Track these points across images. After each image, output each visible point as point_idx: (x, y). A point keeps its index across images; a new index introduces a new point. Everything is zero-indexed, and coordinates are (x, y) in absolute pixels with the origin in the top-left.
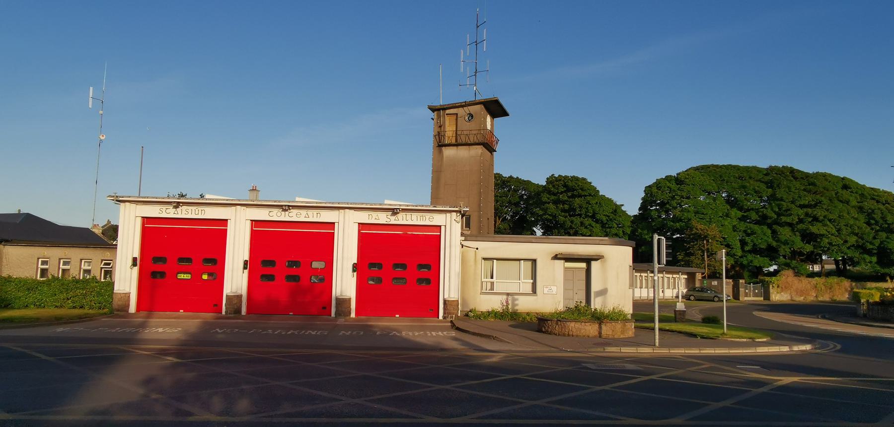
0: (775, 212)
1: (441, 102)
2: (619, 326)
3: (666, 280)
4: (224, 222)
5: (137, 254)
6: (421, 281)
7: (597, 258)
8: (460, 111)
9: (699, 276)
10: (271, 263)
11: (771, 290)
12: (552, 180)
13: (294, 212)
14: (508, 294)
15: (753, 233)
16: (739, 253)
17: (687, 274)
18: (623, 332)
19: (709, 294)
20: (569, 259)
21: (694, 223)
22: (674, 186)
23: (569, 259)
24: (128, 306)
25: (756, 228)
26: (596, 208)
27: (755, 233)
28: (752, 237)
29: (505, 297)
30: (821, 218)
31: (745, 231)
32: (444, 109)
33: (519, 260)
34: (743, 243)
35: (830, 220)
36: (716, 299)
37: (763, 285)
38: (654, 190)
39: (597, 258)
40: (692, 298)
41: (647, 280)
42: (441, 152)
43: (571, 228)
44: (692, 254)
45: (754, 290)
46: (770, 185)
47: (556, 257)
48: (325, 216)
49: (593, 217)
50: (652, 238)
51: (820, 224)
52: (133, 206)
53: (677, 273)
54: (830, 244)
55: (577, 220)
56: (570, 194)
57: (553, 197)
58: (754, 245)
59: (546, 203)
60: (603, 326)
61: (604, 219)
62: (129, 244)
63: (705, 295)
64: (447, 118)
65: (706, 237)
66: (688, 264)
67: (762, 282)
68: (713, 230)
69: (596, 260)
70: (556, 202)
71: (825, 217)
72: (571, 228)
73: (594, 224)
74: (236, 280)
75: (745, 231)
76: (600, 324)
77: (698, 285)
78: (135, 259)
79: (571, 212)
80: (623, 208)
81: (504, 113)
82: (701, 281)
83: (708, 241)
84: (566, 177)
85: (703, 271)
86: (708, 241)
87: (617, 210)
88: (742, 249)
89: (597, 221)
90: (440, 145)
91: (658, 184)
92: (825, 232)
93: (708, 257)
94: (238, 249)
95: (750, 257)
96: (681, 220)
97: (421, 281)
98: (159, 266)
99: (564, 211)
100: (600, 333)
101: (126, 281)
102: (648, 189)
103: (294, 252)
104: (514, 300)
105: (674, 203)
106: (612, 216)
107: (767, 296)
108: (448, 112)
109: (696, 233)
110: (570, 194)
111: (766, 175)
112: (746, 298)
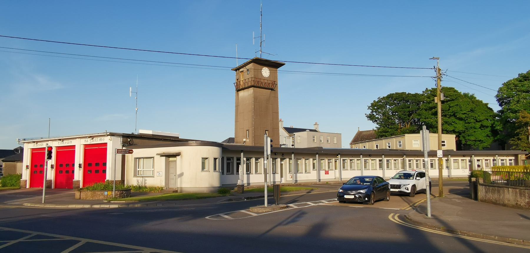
1: (237, 66)
4: (74, 147)
7: (178, 154)
39: (178, 154)
42: (238, 94)
47: (162, 155)
49: (454, 115)
61: (464, 116)
64: (241, 74)
73: (457, 121)
89: (461, 119)
90: (238, 90)
107: (362, 173)
108: (241, 70)
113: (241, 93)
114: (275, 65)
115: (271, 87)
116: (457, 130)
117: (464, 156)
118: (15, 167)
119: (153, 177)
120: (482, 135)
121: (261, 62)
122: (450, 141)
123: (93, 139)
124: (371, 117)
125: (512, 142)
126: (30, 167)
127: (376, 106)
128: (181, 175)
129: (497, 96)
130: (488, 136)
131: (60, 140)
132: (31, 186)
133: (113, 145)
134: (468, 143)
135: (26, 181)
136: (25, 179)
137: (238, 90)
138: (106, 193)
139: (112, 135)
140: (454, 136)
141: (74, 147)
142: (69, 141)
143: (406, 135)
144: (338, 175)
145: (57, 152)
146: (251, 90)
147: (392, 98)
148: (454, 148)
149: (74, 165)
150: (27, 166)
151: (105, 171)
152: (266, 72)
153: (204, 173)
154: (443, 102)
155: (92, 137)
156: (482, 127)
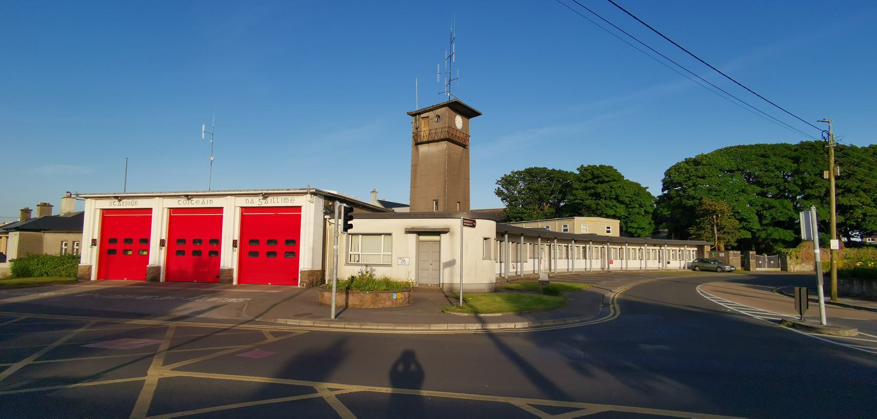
0: (798, 185)
1: (417, 108)
2: (368, 296)
3: (631, 251)
4: (220, 210)
5: (237, 237)
6: (269, 253)
7: (445, 231)
8: (431, 114)
9: (707, 248)
10: (183, 241)
11: (789, 261)
12: (582, 169)
13: (195, 200)
14: (367, 265)
15: (771, 207)
16: (756, 226)
17: (698, 246)
18: (374, 303)
19: (712, 265)
20: (420, 233)
21: (706, 201)
22: (692, 169)
23: (420, 233)
24: (90, 275)
25: (776, 203)
26: (619, 191)
27: (773, 207)
28: (771, 211)
29: (364, 268)
30: (853, 189)
31: (762, 206)
32: (419, 114)
33: (381, 234)
34: (761, 217)
35: (865, 191)
36: (719, 270)
37: (780, 256)
38: (673, 171)
39: (445, 231)
40: (697, 268)
41: (597, 252)
42: (417, 149)
43: (597, 209)
44: (704, 229)
45: (769, 260)
46: (796, 160)
47: (409, 231)
48: (216, 203)
49: (617, 198)
50: (333, 205)
51: (851, 195)
52: (93, 200)
53: (683, 246)
54: (865, 215)
55: (602, 202)
56: (596, 180)
57: (583, 185)
58: (773, 218)
59: (577, 189)
60: (351, 297)
61: (627, 200)
62: (92, 228)
63: (708, 266)
64: (423, 122)
65: (714, 212)
66: (699, 237)
67: (779, 253)
68: (723, 206)
69: (445, 232)
70: (585, 189)
71: (858, 187)
72: (597, 209)
73: (618, 205)
74: (157, 256)
75: (762, 206)
76: (347, 293)
77: (706, 256)
78: (235, 242)
79: (597, 196)
80: (648, 190)
81: (476, 114)
82: (710, 253)
83: (717, 216)
84: (594, 167)
85: (713, 243)
86: (717, 216)
87: (639, 191)
88: (760, 222)
89: (622, 203)
90: (417, 144)
91: (677, 168)
92: (857, 203)
93: (718, 230)
94: (159, 230)
95: (770, 229)
96: (694, 198)
97: (269, 253)
98: (113, 246)
99: (591, 195)
100: (347, 303)
101: (89, 257)
102: (668, 173)
103: (195, 230)
104: (372, 271)
105: (690, 183)
106: (634, 198)
107: (784, 267)
108: (422, 116)
109: (705, 209)
110: (596, 180)
111: (796, 150)
112: (758, 269)
113: (423, 149)
114: (469, 113)
115: (460, 141)
116: (618, 215)
117: (655, 245)
118: (40, 241)
119: (390, 265)
120: (646, 222)
121: (458, 108)
122: (613, 227)
123: (120, 201)
124: (499, 193)
125: (692, 232)
126: (98, 243)
127: (507, 181)
128: (451, 263)
129: (663, 181)
130: (650, 224)
131: (187, 196)
132: (100, 275)
133: (311, 212)
134: (630, 230)
135: (90, 267)
136: (88, 264)
137: (417, 144)
138: (395, 296)
139: (316, 193)
140: (618, 221)
141: (220, 210)
142: (209, 199)
143: (576, 218)
144: (544, 265)
145: (170, 217)
146: (444, 145)
147: (531, 174)
148: (618, 235)
149: (218, 241)
150: (94, 241)
151: (296, 253)
152: (459, 121)
153: (487, 262)
154: (837, 178)
155: (188, 197)
156: (646, 212)
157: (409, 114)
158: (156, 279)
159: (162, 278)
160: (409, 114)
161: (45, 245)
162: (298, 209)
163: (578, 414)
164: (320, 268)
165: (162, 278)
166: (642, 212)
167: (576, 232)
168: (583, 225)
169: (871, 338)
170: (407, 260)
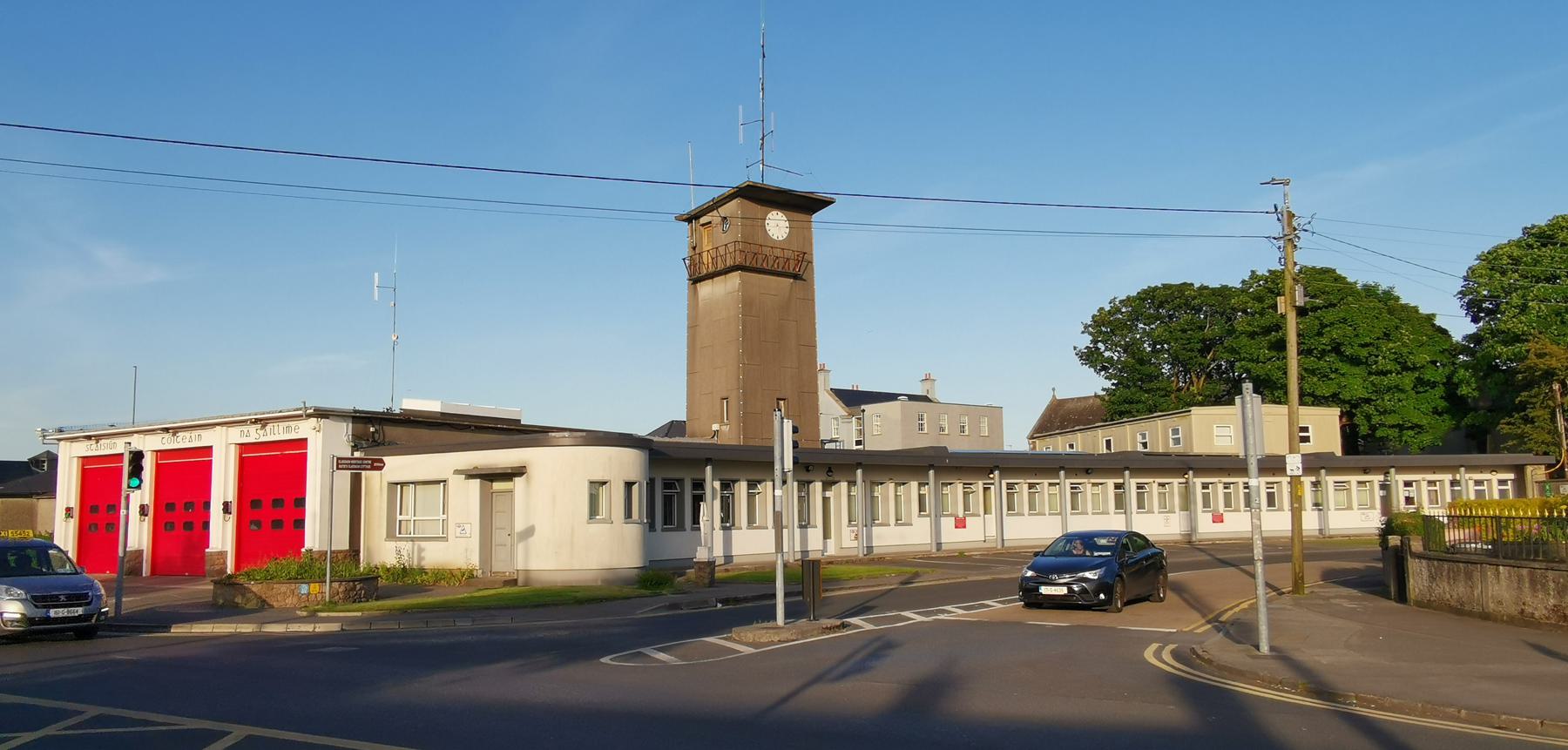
1: (693, 206)
4: (208, 450)
49: (1337, 349)
64: (705, 232)
73: (1345, 368)
89: (1355, 361)
90: (696, 280)
104: (421, 550)
107: (1128, 522)
108: (703, 220)
113: (705, 289)
114: (804, 205)
115: (794, 268)
117: (1366, 471)
119: (445, 539)
120: (1418, 409)
121: (761, 196)
123: (264, 426)
124: (1090, 357)
131: (166, 430)
133: (324, 446)
137: (696, 280)
138: (304, 589)
139: (322, 414)
140: (1336, 411)
141: (208, 450)
145: (158, 465)
146: (735, 279)
148: (1336, 447)
149: (207, 504)
151: (300, 523)
152: (777, 225)
153: (595, 528)
154: (1301, 312)
155: (262, 422)
157: (680, 218)
158: (136, 571)
159: (146, 569)
160: (680, 218)
161: (39, 519)
162: (302, 443)
163: (228, 741)
164: (346, 547)
165: (146, 569)
166: (1408, 380)
167: (1197, 450)
168: (1213, 429)
169: (547, 628)
170: (467, 527)
